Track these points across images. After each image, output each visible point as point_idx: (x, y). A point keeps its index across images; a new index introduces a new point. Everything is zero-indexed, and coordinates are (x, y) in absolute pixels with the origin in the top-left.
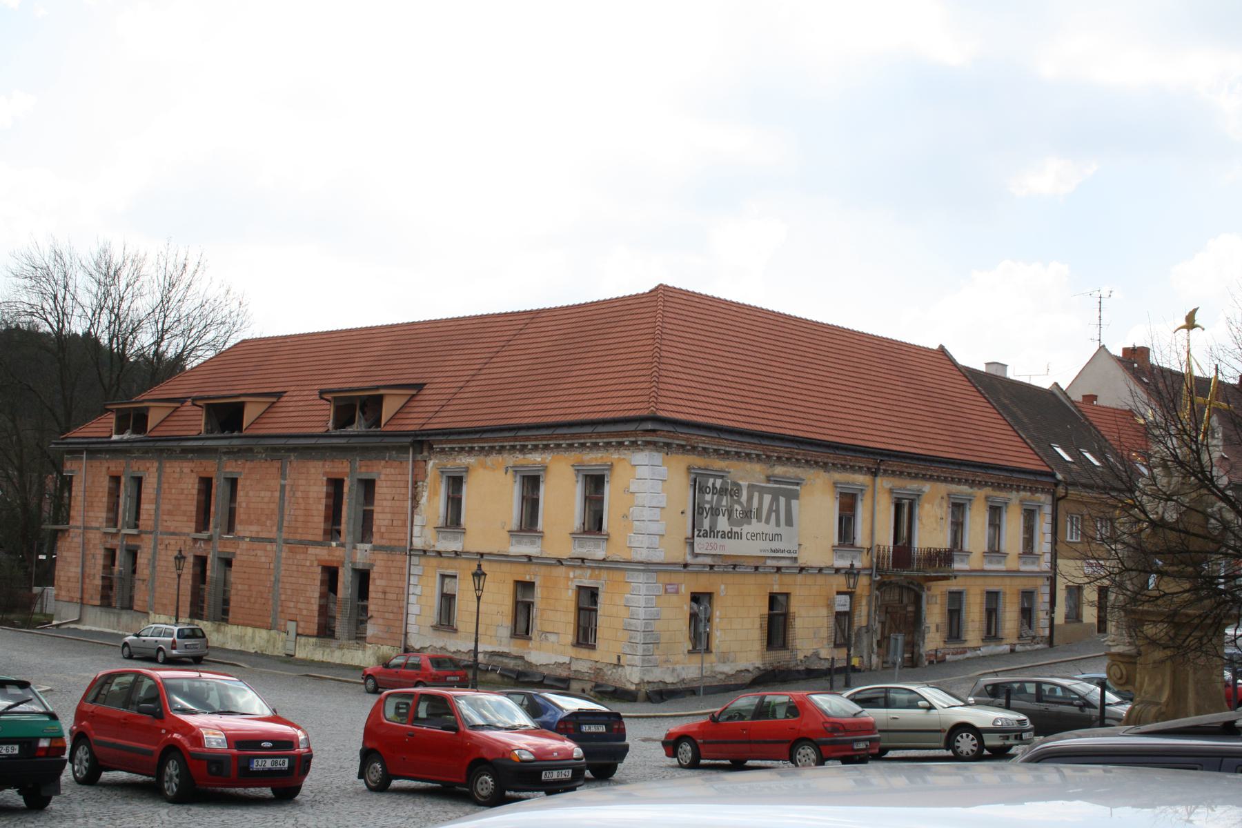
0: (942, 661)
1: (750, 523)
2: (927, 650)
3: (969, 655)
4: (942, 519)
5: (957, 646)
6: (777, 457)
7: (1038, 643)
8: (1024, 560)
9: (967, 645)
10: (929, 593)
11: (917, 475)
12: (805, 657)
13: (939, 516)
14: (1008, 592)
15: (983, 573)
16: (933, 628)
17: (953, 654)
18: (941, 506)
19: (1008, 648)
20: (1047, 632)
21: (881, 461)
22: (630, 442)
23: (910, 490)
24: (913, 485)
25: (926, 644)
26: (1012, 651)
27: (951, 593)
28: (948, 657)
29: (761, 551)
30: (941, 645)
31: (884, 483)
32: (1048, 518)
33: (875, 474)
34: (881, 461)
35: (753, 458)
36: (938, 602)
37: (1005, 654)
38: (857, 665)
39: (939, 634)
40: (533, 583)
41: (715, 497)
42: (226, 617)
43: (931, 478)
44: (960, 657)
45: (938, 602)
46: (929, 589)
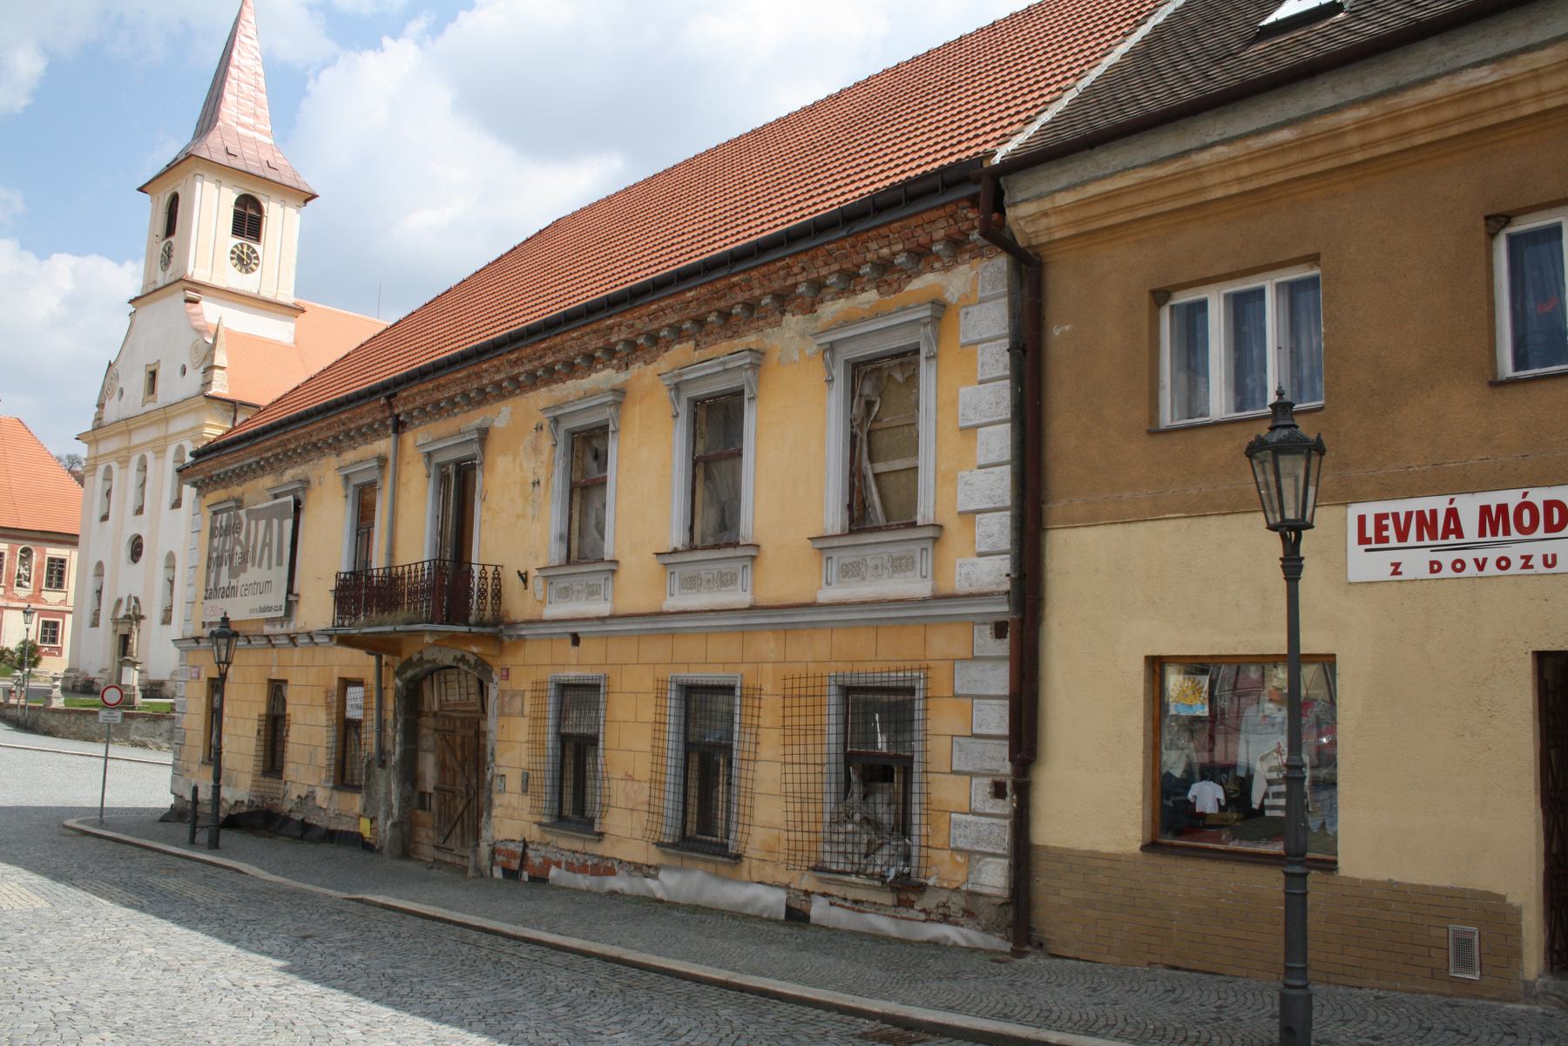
2: (500, 837)
3: (617, 883)
4: (536, 483)
5: (578, 845)
6: (841, 271)
7: (946, 919)
10: (505, 685)
11: (532, 375)
12: (299, 797)
14: (768, 688)
16: (514, 782)
17: (571, 867)
19: (773, 900)
20: (994, 877)
25: (495, 821)
26: (796, 916)
30: (535, 833)
32: (996, 360)
36: (527, 710)
37: (758, 918)
44: (584, 881)
45: (527, 710)
46: (506, 674)
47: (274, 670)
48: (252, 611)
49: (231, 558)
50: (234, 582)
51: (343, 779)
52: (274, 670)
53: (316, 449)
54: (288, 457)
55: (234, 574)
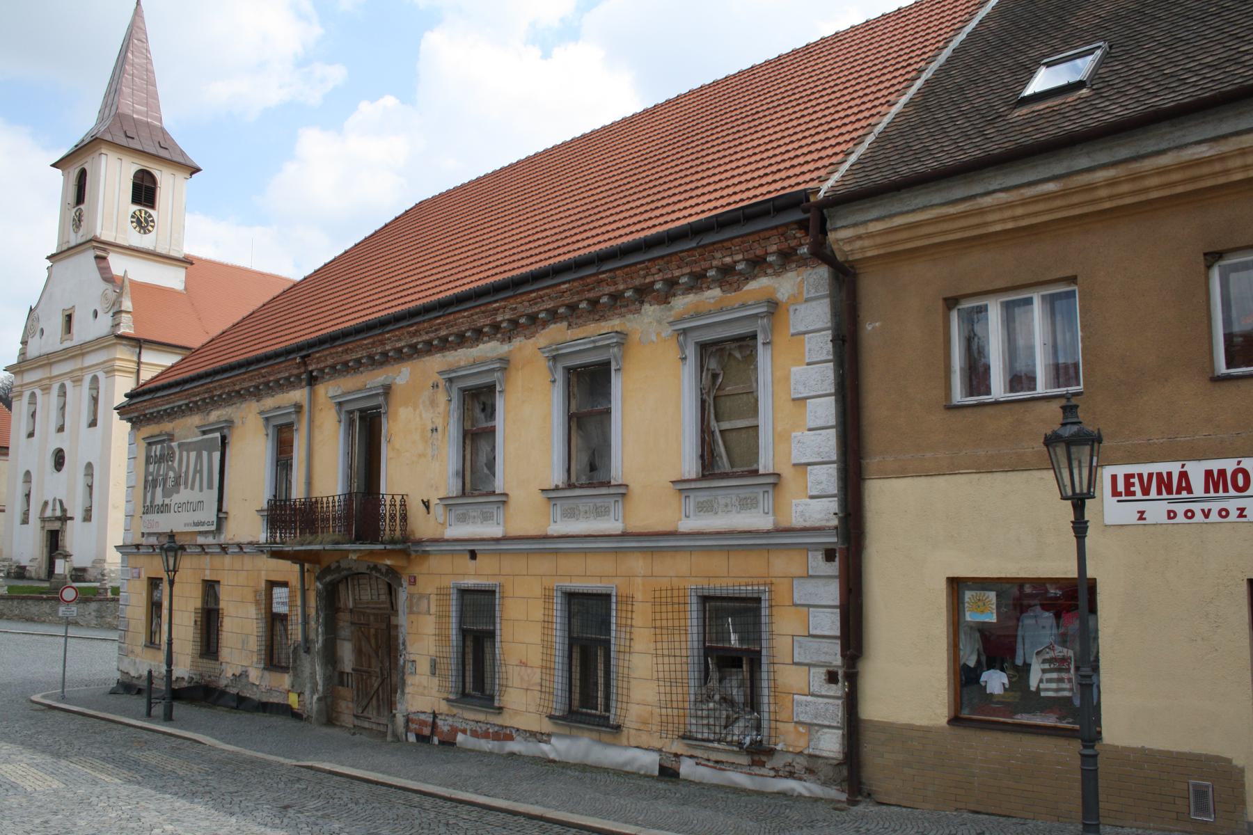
0: (448, 743)
1: (178, 492)
2: (413, 709)
3: (515, 746)
4: (434, 430)
5: (481, 717)
8: (460, 511)
9: (506, 720)
10: (413, 589)
13: (429, 428)
14: (639, 596)
15: (543, 545)
16: (424, 666)
17: (475, 734)
18: (433, 403)
21: (303, 357)
22: (691, 274)
23: (370, 389)
24: (375, 379)
25: (408, 697)
26: (668, 773)
27: (464, 592)
28: (460, 738)
29: (185, 525)
31: (328, 390)
32: (821, 346)
33: (312, 381)
34: (303, 357)
35: (770, 265)
38: (295, 706)
39: (436, 680)
40: (760, 598)
41: (156, 465)
42: (117, 597)
43: (401, 356)
44: (487, 745)
45: (433, 609)
46: (413, 581)
47: (207, 572)
48: (186, 525)
49: (165, 481)
50: (167, 501)
51: (272, 660)
52: (207, 572)
53: (239, 396)
54: (213, 402)
55: (167, 494)
